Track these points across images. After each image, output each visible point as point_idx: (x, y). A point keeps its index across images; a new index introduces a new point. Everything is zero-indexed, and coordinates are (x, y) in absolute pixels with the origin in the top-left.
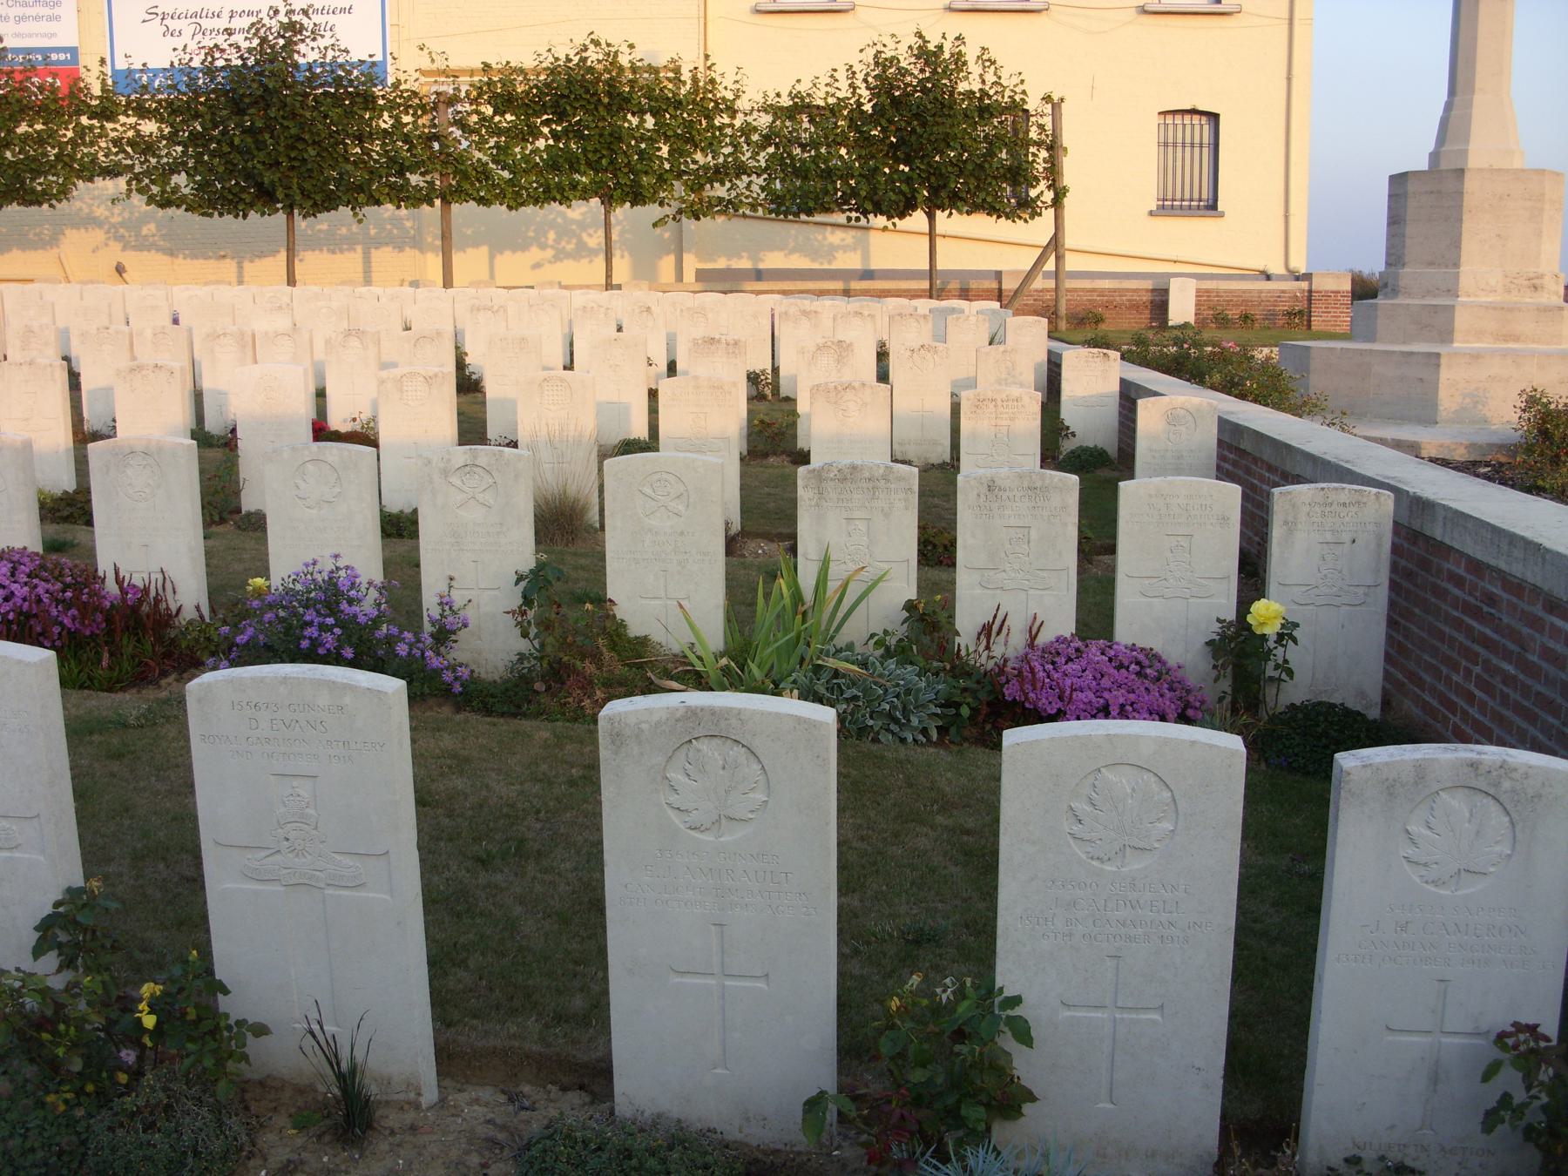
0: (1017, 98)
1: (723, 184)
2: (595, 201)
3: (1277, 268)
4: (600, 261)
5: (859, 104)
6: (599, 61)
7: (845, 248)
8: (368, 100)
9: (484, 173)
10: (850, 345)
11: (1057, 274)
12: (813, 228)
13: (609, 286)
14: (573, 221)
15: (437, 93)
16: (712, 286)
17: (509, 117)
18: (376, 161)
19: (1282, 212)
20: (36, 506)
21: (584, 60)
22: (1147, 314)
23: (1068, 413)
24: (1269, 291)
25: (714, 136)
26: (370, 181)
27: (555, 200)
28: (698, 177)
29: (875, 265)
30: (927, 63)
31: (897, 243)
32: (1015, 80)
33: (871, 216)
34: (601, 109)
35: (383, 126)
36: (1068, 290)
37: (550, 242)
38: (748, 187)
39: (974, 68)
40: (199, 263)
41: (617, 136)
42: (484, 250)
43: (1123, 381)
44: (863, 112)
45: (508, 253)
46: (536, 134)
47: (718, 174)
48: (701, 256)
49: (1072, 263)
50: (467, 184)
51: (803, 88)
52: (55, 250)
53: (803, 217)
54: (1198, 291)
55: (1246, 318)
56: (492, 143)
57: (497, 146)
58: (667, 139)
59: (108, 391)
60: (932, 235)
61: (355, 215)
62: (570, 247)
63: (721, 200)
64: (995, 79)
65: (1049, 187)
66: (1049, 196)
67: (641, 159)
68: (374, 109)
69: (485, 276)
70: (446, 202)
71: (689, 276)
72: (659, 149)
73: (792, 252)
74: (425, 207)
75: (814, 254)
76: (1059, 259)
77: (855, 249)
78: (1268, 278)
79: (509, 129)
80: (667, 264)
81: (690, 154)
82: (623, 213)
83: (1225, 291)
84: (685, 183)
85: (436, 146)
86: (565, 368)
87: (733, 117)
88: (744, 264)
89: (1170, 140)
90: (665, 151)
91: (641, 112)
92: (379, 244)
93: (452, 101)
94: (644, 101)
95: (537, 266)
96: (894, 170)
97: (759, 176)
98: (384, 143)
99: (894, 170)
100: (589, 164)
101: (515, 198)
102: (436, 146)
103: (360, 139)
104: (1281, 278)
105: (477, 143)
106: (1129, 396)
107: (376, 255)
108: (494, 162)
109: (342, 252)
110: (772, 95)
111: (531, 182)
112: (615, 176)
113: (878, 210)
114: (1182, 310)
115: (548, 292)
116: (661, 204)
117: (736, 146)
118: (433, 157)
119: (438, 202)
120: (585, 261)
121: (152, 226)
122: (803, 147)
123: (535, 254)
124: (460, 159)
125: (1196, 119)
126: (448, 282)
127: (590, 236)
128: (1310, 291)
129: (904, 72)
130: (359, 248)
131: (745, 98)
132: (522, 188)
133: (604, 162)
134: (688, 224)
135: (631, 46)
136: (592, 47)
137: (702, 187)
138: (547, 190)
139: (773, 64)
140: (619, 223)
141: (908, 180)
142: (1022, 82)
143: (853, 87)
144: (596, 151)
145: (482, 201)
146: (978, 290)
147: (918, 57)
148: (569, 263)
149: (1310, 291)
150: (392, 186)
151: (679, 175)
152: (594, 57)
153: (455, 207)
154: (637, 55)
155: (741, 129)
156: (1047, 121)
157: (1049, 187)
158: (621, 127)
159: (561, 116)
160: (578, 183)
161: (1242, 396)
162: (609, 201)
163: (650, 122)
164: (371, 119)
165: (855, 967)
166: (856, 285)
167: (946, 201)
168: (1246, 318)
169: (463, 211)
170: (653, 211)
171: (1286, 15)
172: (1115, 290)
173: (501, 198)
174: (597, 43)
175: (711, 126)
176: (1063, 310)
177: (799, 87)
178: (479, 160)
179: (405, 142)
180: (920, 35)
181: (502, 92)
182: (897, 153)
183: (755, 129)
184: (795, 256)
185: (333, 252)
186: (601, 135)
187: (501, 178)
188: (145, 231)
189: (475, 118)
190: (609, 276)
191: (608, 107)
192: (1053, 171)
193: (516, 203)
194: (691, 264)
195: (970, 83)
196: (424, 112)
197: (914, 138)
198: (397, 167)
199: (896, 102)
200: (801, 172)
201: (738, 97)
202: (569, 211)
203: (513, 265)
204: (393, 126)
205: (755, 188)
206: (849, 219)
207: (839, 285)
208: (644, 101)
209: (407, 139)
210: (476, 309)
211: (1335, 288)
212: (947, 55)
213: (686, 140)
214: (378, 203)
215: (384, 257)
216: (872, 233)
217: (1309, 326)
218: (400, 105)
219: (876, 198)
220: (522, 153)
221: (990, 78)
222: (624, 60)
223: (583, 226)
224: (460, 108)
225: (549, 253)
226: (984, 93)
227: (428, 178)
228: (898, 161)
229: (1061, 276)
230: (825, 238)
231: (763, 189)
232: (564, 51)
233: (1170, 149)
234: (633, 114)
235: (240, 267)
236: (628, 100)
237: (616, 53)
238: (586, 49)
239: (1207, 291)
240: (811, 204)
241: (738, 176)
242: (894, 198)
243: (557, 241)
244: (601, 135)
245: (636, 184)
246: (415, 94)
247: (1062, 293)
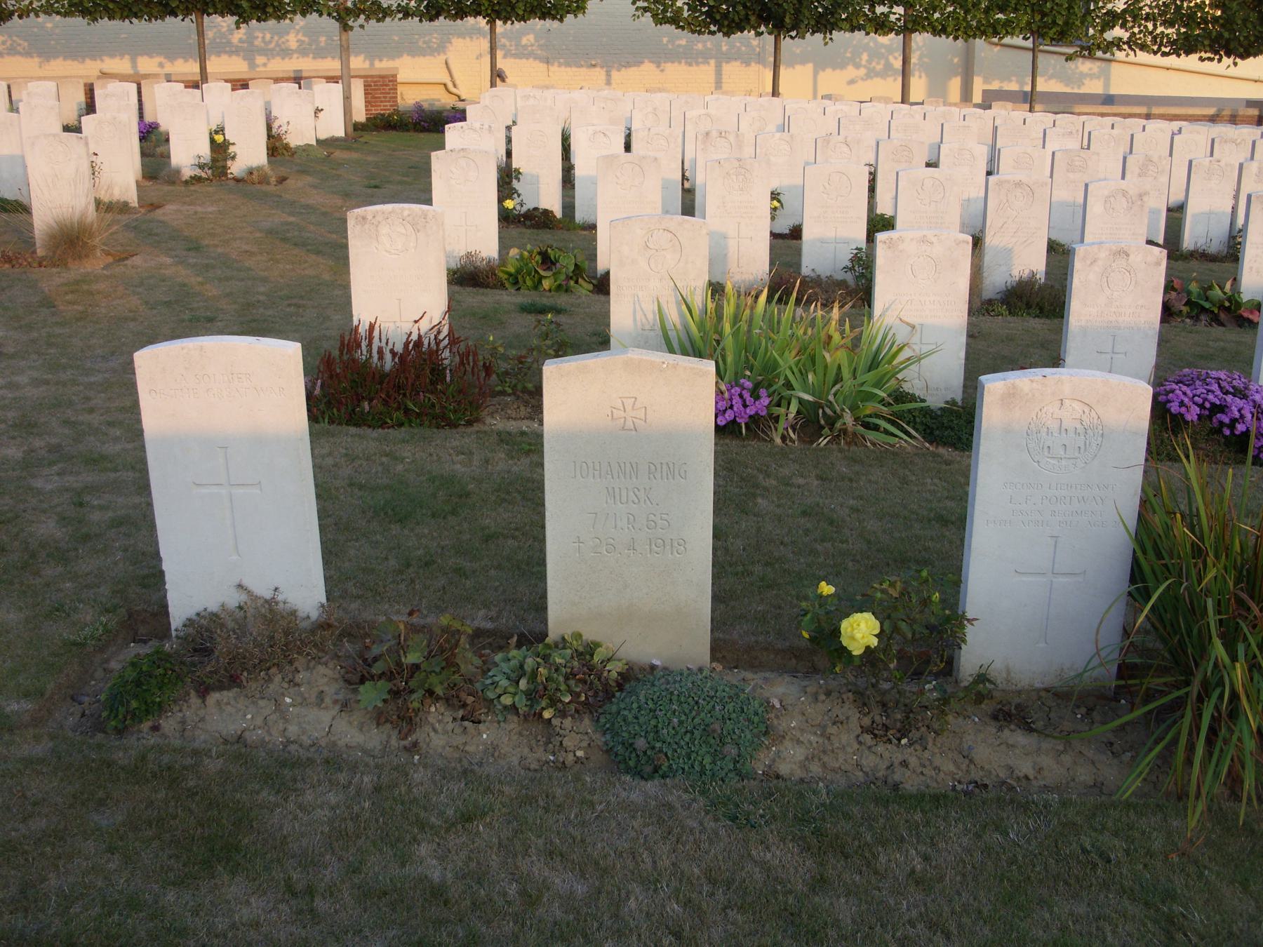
7: (1092, 76)
14: (883, 46)
20: (445, 273)
29: (1114, 90)
37: (864, 63)
40: (572, 71)
42: (810, 66)
45: (829, 71)
48: (987, 80)
52: (442, 58)
53: (1099, 54)
59: (594, 182)
62: (879, 67)
73: (1051, 77)
75: (1067, 80)
77: (1098, 78)
80: (955, 85)
86: (928, 165)
92: (729, 59)
95: (851, 82)
107: (727, 68)
109: (698, 64)
121: (531, 37)
123: (851, 72)
130: (712, 62)
140: (919, 48)
146: (1243, 116)
148: (878, 81)
165: (717, 635)
184: (1053, 82)
185: (690, 65)
188: (524, 41)
203: (832, 80)
207: (1143, 110)
215: (732, 70)
216: (1114, 65)
223: (890, 50)
225: (863, 71)
235: (608, 75)
243: (869, 62)
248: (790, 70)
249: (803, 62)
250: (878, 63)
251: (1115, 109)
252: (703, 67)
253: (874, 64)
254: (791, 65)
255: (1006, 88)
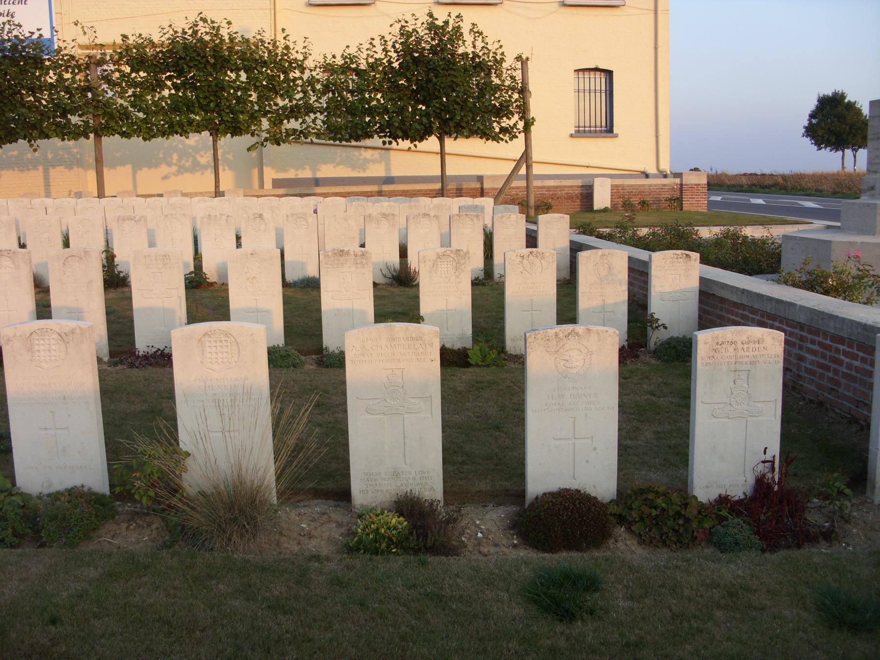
0: (498, 57)
1: (297, 120)
2: (206, 134)
3: (652, 170)
4: (210, 175)
5: (390, 62)
6: (207, 33)
7: (374, 161)
8: (37, 62)
9: (125, 114)
10: (467, 253)
11: (528, 176)
12: (352, 149)
13: (218, 193)
14: (190, 147)
15: (90, 57)
16: (292, 191)
17: (142, 74)
18: (45, 106)
19: (654, 133)
21: (195, 32)
22: (578, 202)
23: (657, 307)
24: (656, 185)
25: (289, 86)
26: (41, 121)
27: (177, 133)
28: (279, 115)
29: (394, 173)
30: (435, 33)
31: (415, 159)
32: (496, 46)
33: (400, 141)
34: (209, 67)
35: (50, 80)
36: (536, 187)
37: (174, 161)
38: (314, 121)
39: (468, 38)
41: (221, 87)
42: (129, 168)
43: (702, 279)
44: (393, 68)
45: (145, 169)
46: (162, 86)
47: (294, 112)
49: (537, 170)
50: (110, 122)
51: (352, 51)
54: (612, 186)
55: (643, 203)
56: (130, 92)
57: (134, 95)
58: (256, 88)
60: (442, 153)
61: (31, 146)
62: (188, 164)
63: (295, 130)
64: (483, 44)
65: (520, 119)
66: (521, 125)
67: (238, 103)
68: (42, 68)
69: (130, 187)
70: (98, 136)
71: (268, 185)
72: (251, 96)
73: (338, 164)
74: (82, 139)
76: (528, 167)
78: (647, 176)
79: (142, 83)
81: (272, 99)
82: (226, 141)
83: (628, 186)
84: (269, 120)
85: (90, 95)
87: (302, 73)
88: (307, 174)
89: (581, 88)
90: (254, 97)
91: (237, 70)
93: (101, 62)
94: (239, 62)
95: (165, 178)
96: (415, 109)
97: (321, 113)
98: (50, 94)
99: (415, 109)
100: (201, 107)
101: (148, 132)
102: (90, 95)
103: (32, 90)
104: (655, 176)
105: (119, 93)
106: (639, 276)
108: (131, 106)
109: (29, 170)
110: (329, 57)
111: (161, 121)
112: (220, 115)
113: (405, 137)
114: (602, 199)
115: (175, 200)
116: (253, 135)
117: (305, 92)
118: (87, 103)
119: (92, 136)
120: (198, 174)
122: (352, 92)
123: (164, 169)
124: (108, 104)
125: (598, 73)
126: (101, 194)
127: (202, 156)
128: (681, 185)
129: (419, 41)
130: (41, 168)
131: (310, 58)
132: (153, 125)
133: (212, 105)
134: (270, 147)
135: (229, 23)
136: (201, 23)
137: (281, 122)
138: (171, 126)
139: (326, 39)
141: (427, 115)
142: (501, 47)
143: (385, 50)
144: (205, 98)
145: (124, 135)
146: (467, 189)
147: (429, 29)
148: (187, 175)
149: (681, 185)
150: (58, 125)
151: (265, 115)
152: (203, 30)
153: (104, 139)
154: (234, 29)
155: (308, 80)
156: (518, 75)
157: (520, 119)
158: (224, 80)
159: (180, 73)
160: (194, 120)
161: (826, 293)
162: (216, 133)
163: (243, 76)
164: (40, 76)
166: (386, 188)
167: (453, 129)
168: (643, 203)
169: (111, 142)
170: (246, 140)
171: (652, 7)
172: (557, 187)
173: (138, 132)
174: (204, 20)
175: (287, 79)
176: (532, 202)
177: (348, 51)
178: (121, 105)
179: (66, 92)
180: (430, 15)
181: (136, 56)
182: (414, 97)
183: (318, 81)
185: (23, 171)
186: (209, 86)
187: (137, 118)
189: (117, 75)
190: (217, 186)
191: (214, 66)
192: (524, 111)
193: (149, 135)
194: (270, 174)
195: (465, 47)
196: (80, 71)
197: (430, 85)
198: (61, 110)
199: (416, 61)
200: (352, 110)
201: (305, 58)
202: (187, 141)
203: (149, 179)
204: (57, 81)
205: (319, 122)
206: (384, 143)
207: (374, 188)
208: (239, 62)
209: (67, 90)
210: (122, 219)
211: (697, 182)
212: (450, 29)
213: (272, 89)
214: (47, 137)
215: (58, 174)
217: (682, 209)
218: (61, 66)
219: (404, 128)
220: (152, 99)
221: (479, 44)
222: (224, 32)
224: (105, 67)
225: (174, 169)
226: (476, 55)
227: (84, 118)
228: (418, 102)
229: (531, 178)
230: (360, 155)
231: (324, 122)
232: (181, 25)
233: (581, 94)
234: (232, 72)
236: (227, 61)
237: (219, 27)
238: (197, 26)
239: (617, 186)
240: (360, 132)
241: (307, 114)
242: (418, 127)
243: (179, 160)
244: (209, 86)
245: (235, 120)
246: (72, 57)
247: (532, 190)
248: (112, 171)
249: (123, 163)
250: (187, 161)
251: (319, 190)
252: (33, 173)
253: (183, 162)
254: (113, 166)
255: (300, 176)
